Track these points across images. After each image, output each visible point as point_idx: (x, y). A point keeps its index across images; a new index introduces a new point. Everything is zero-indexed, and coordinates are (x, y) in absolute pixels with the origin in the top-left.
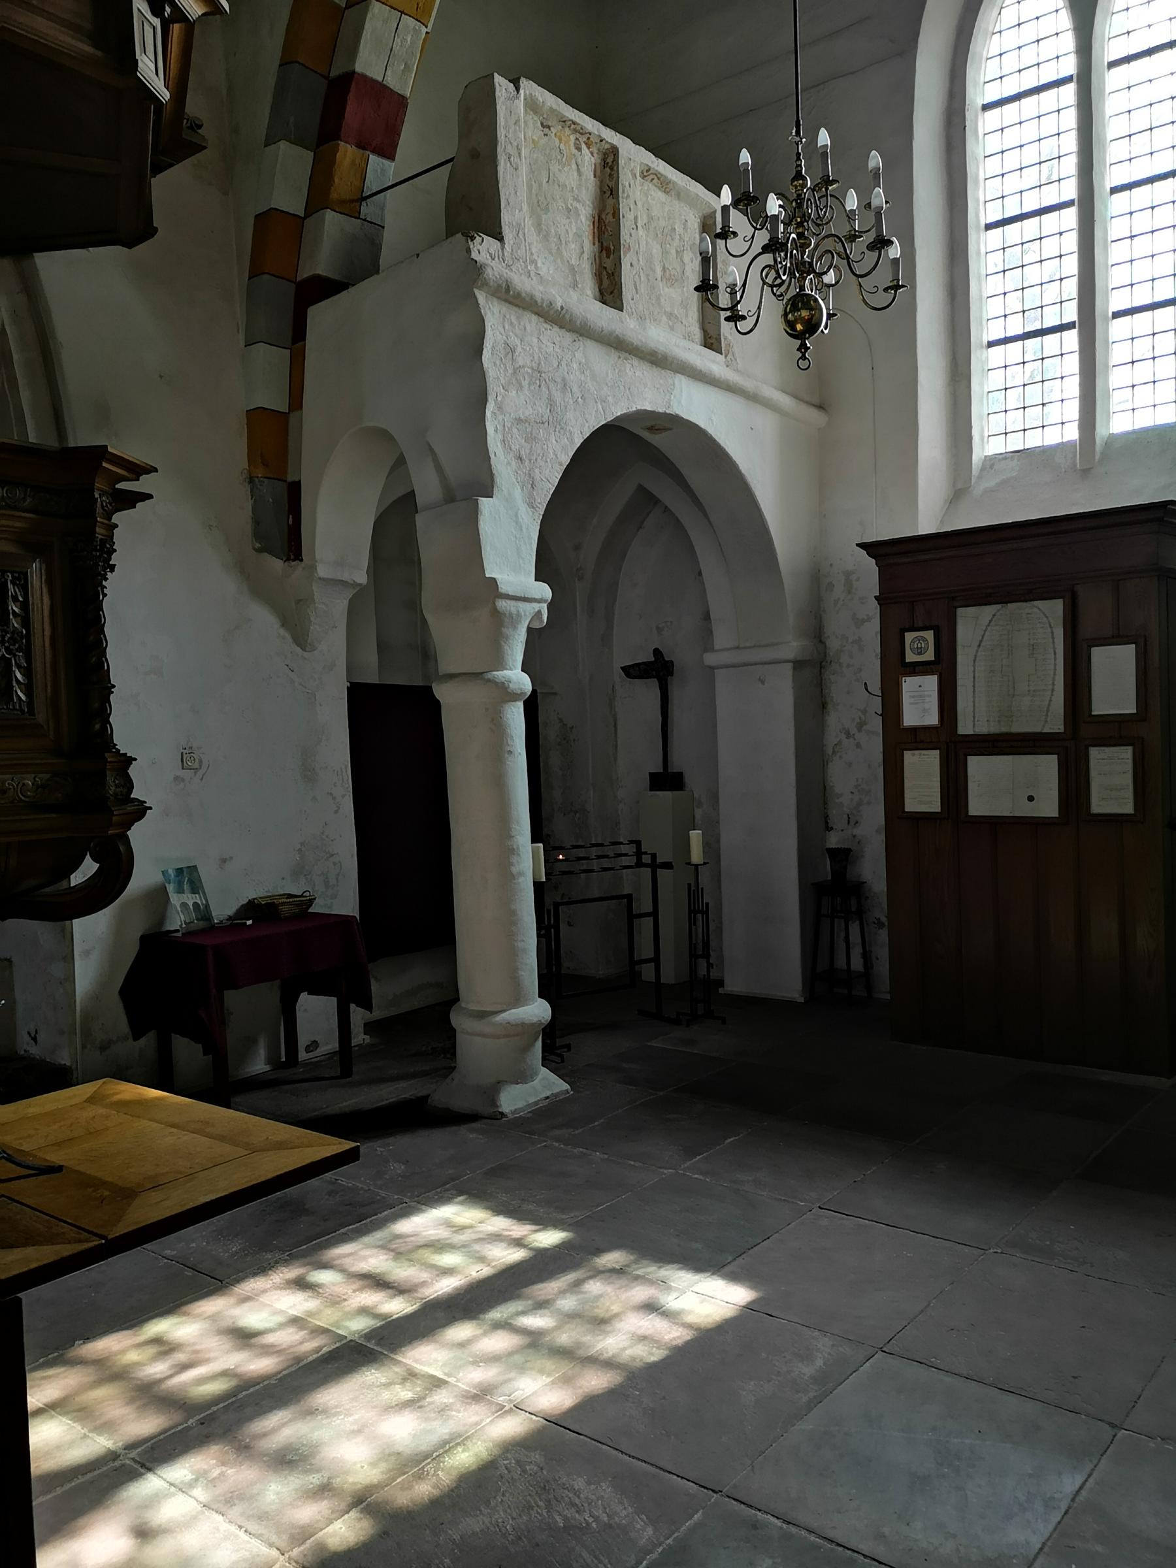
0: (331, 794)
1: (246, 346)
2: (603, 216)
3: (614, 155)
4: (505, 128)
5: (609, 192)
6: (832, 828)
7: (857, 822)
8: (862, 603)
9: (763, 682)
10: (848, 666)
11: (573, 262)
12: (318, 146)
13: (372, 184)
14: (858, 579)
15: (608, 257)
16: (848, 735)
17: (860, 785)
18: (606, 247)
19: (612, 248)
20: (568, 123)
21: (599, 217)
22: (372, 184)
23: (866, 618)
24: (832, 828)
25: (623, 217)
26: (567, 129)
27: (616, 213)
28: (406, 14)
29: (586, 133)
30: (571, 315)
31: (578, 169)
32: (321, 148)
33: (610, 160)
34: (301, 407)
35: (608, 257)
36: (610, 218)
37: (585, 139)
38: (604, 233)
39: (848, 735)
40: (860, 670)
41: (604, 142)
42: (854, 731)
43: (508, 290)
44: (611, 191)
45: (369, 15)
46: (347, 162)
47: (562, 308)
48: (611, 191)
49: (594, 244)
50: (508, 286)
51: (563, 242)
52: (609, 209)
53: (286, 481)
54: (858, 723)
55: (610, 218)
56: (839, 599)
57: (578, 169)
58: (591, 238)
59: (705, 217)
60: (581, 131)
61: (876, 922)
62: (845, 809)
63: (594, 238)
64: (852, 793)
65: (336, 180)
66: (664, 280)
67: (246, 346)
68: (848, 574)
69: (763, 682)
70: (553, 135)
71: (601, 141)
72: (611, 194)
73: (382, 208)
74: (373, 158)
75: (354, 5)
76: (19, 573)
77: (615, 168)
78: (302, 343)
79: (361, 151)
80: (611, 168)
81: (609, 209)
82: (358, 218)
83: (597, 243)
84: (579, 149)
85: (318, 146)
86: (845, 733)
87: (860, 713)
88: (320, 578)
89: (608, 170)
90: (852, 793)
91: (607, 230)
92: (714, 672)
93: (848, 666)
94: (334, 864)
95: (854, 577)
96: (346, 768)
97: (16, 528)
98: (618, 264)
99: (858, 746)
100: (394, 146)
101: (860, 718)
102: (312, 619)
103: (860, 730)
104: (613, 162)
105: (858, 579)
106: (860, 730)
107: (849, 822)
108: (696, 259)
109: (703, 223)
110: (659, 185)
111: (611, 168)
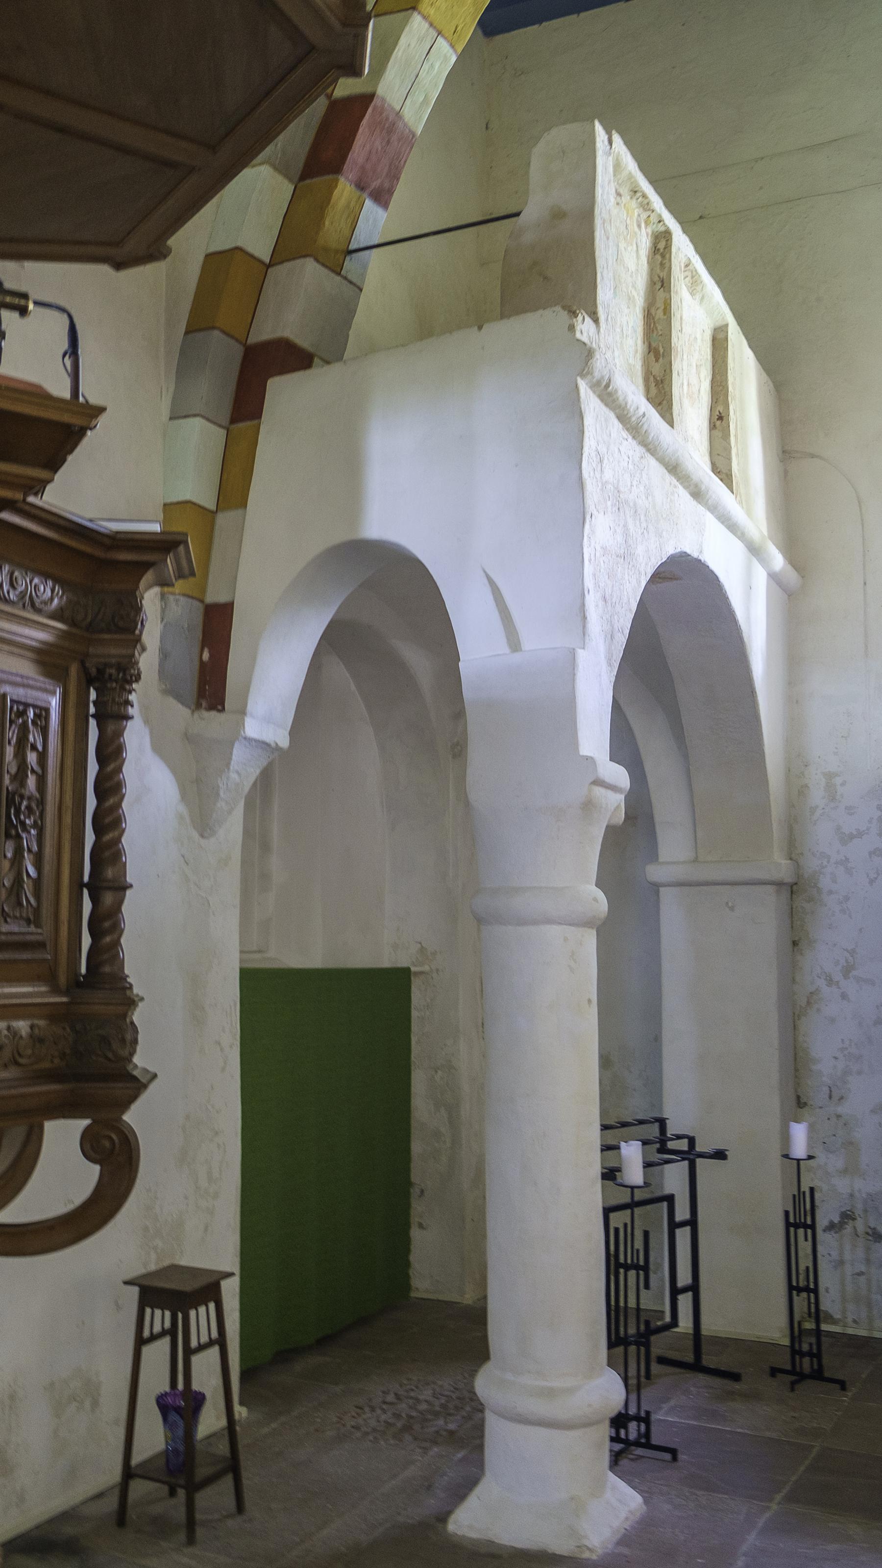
0: (219, 1044)
1: (171, 419)
2: (653, 311)
3: (667, 241)
4: (602, 187)
5: (660, 284)
6: (805, 1104)
7: (842, 1098)
8: (851, 814)
9: (732, 909)
10: (830, 892)
11: (630, 361)
12: (303, 178)
13: (364, 234)
14: (843, 784)
15: (657, 361)
16: (830, 981)
17: (847, 1049)
18: (655, 348)
19: (661, 350)
20: (638, 194)
21: (648, 311)
22: (364, 234)
23: (855, 833)
24: (805, 1104)
25: (674, 315)
26: (634, 201)
27: (667, 309)
28: (443, 36)
29: (649, 210)
30: (649, 426)
31: (637, 250)
32: (308, 181)
33: (661, 246)
34: (243, 504)
35: (657, 361)
36: (660, 314)
37: (645, 217)
38: (653, 331)
39: (830, 981)
40: (847, 898)
41: (662, 223)
42: (837, 976)
43: (608, 385)
44: (662, 281)
45: (407, 29)
46: (342, 202)
47: (644, 415)
48: (662, 281)
49: (644, 343)
50: (610, 380)
51: (625, 336)
52: (660, 304)
53: (202, 601)
54: (843, 967)
55: (660, 314)
56: (817, 807)
57: (637, 250)
58: (642, 334)
59: (715, 330)
60: (646, 206)
61: (871, 1233)
62: (824, 1079)
63: (644, 334)
64: (836, 1058)
65: (327, 223)
66: (688, 397)
67: (171, 419)
68: (830, 776)
69: (732, 909)
70: (623, 205)
71: (660, 222)
72: (662, 286)
73: (365, 267)
74: (369, 203)
75: (385, 14)
76: (41, 708)
77: (667, 256)
78: (255, 422)
79: (358, 193)
80: (663, 256)
81: (660, 304)
82: (339, 274)
83: (646, 342)
84: (639, 226)
85: (303, 178)
86: (826, 979)
87: (848, 955)
88: (245, 738)
89: (658, 257)
90: (836, 1058)
91: (656, 329)
92: (659, 890)
93: (830, 892)
94: (219, 1146)
95: (838, 781)
96: (235, 1005)
97: (32, 639)
98: (668, 371)
99: (844, 996)
100: (390, 192)
101: (847, 961)
102: (222, 794)
103: (846, 976)
104: (665, 248)
105: (843, 784)
106: (846, 976)
107: (830, 1097)
108: (708, 377)
109: (713, 337)
110: (690, 284)
111: (663, 256)
